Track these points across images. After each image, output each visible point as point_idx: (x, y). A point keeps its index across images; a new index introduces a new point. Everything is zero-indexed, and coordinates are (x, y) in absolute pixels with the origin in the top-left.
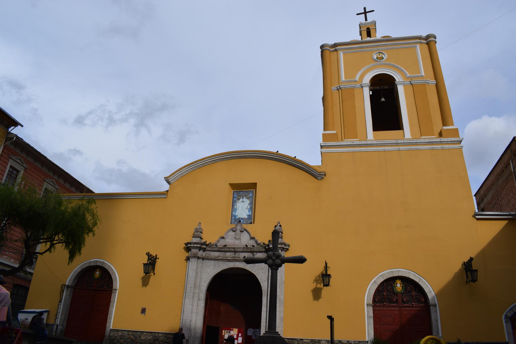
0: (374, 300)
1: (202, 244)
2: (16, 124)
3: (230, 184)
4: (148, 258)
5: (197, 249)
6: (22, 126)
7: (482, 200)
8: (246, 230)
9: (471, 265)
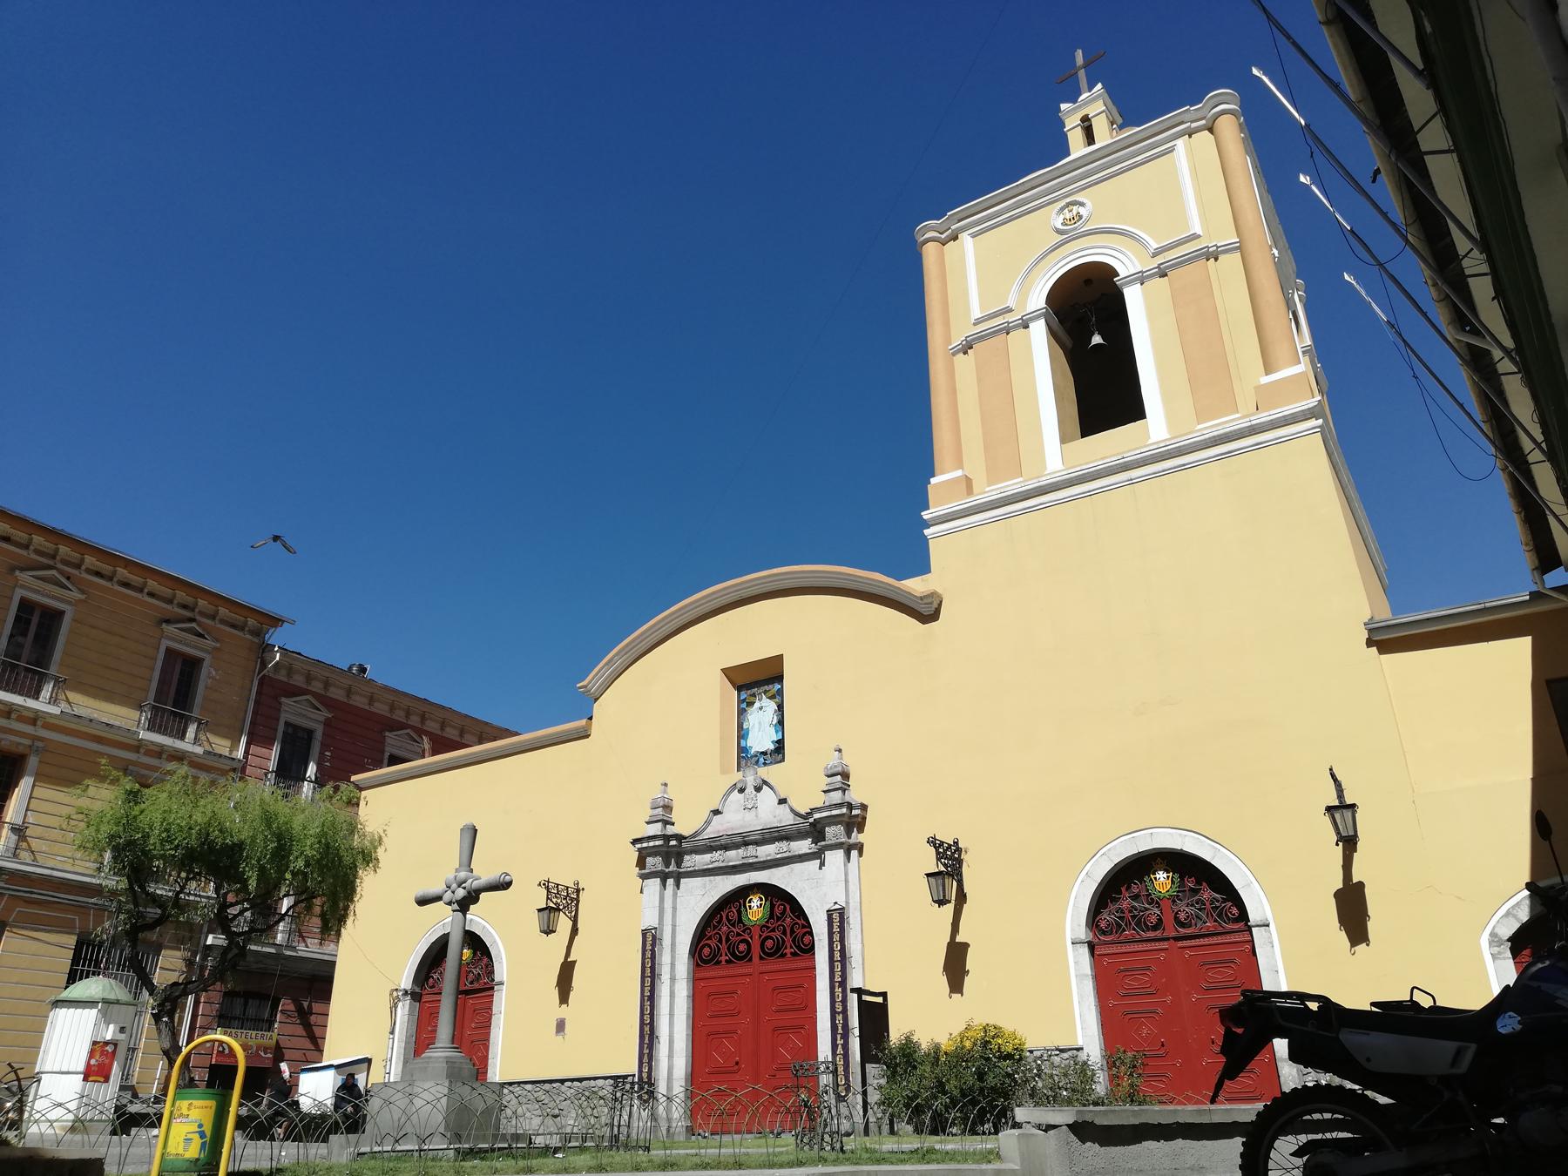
1: (667, 838)
2: (276, 621)
4: (938, 853)
5: (665, 856)
6: (293, 622)
8: (765, 782)
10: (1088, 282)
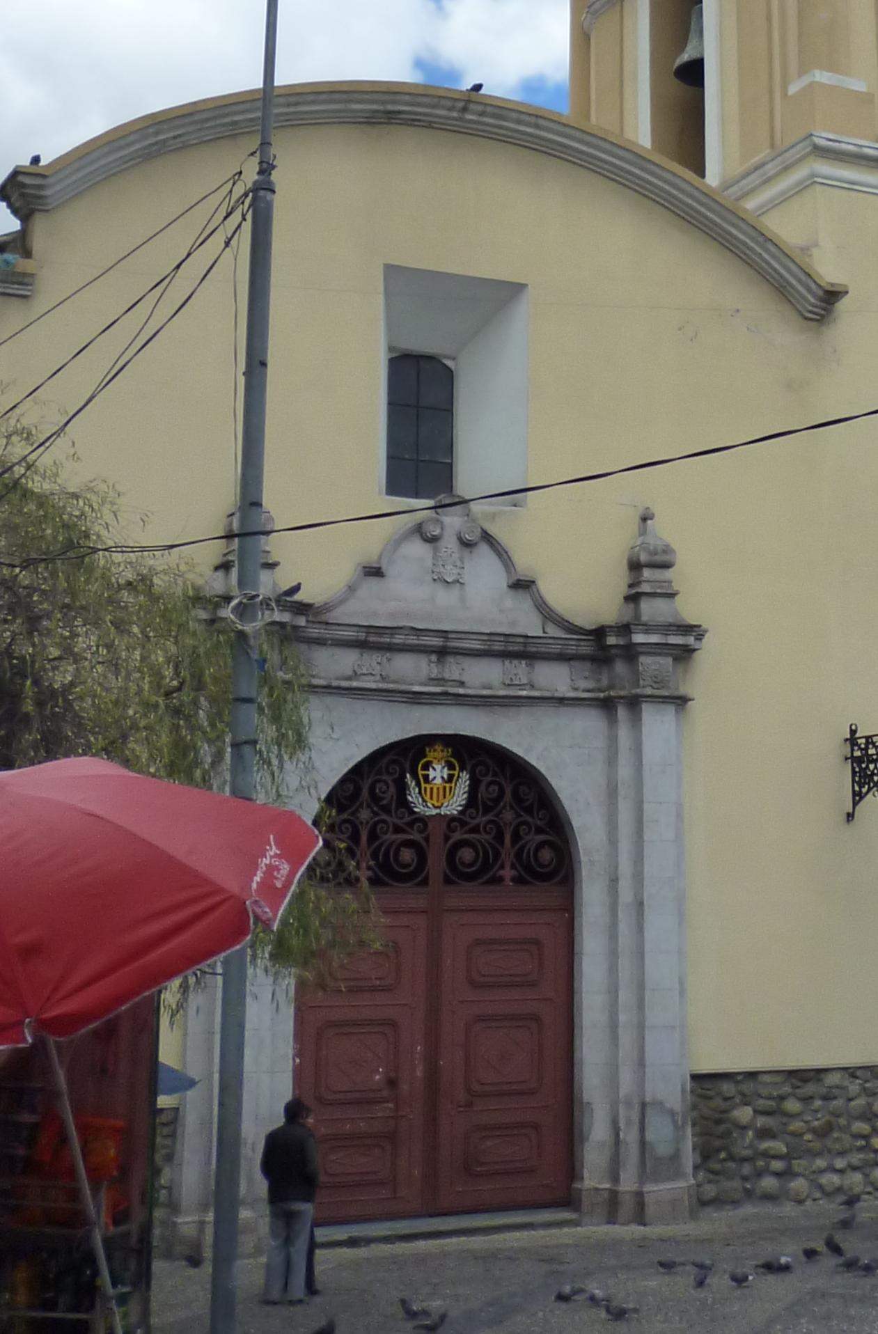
8: (487, 537)
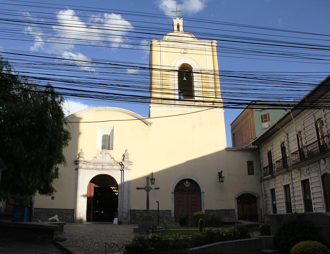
0: (175, 191)
3: (159, 188)
7: (234, 128)
9: (221, 174)
10: (184, 66)
